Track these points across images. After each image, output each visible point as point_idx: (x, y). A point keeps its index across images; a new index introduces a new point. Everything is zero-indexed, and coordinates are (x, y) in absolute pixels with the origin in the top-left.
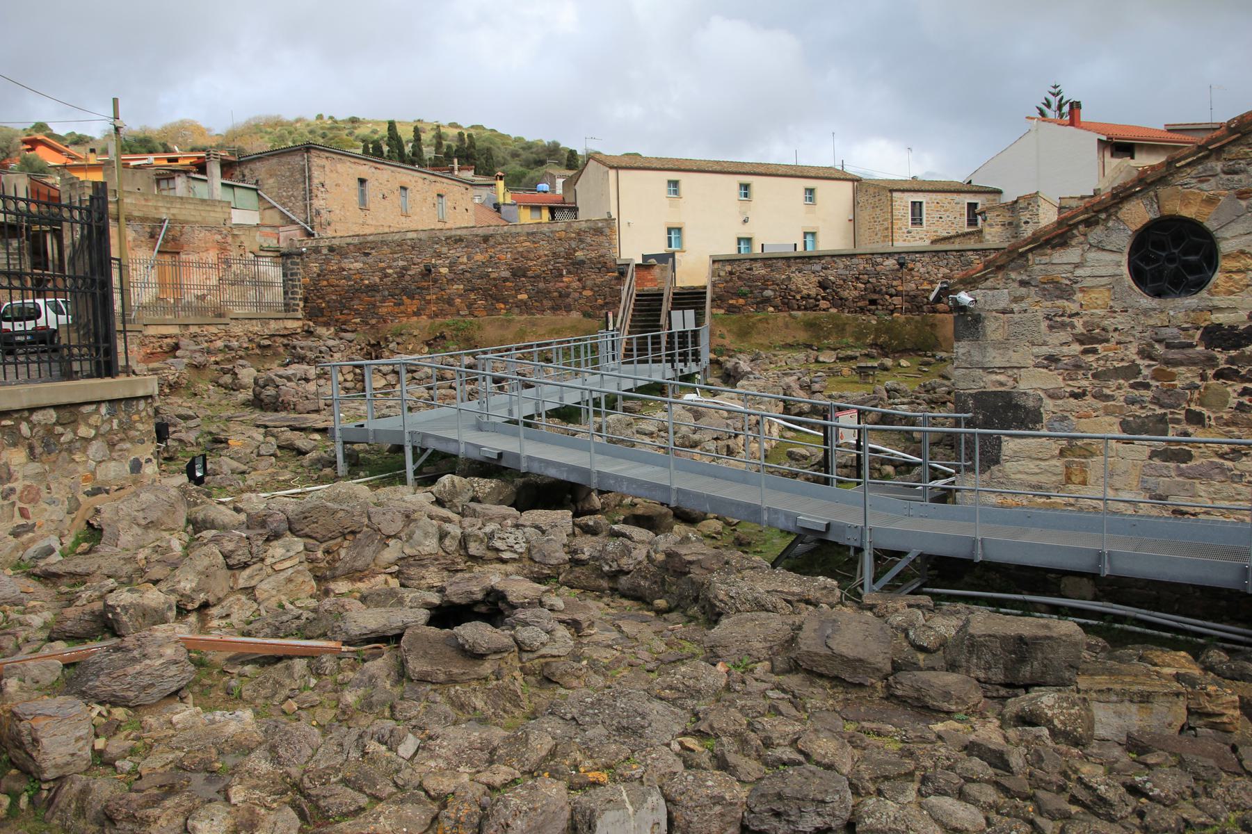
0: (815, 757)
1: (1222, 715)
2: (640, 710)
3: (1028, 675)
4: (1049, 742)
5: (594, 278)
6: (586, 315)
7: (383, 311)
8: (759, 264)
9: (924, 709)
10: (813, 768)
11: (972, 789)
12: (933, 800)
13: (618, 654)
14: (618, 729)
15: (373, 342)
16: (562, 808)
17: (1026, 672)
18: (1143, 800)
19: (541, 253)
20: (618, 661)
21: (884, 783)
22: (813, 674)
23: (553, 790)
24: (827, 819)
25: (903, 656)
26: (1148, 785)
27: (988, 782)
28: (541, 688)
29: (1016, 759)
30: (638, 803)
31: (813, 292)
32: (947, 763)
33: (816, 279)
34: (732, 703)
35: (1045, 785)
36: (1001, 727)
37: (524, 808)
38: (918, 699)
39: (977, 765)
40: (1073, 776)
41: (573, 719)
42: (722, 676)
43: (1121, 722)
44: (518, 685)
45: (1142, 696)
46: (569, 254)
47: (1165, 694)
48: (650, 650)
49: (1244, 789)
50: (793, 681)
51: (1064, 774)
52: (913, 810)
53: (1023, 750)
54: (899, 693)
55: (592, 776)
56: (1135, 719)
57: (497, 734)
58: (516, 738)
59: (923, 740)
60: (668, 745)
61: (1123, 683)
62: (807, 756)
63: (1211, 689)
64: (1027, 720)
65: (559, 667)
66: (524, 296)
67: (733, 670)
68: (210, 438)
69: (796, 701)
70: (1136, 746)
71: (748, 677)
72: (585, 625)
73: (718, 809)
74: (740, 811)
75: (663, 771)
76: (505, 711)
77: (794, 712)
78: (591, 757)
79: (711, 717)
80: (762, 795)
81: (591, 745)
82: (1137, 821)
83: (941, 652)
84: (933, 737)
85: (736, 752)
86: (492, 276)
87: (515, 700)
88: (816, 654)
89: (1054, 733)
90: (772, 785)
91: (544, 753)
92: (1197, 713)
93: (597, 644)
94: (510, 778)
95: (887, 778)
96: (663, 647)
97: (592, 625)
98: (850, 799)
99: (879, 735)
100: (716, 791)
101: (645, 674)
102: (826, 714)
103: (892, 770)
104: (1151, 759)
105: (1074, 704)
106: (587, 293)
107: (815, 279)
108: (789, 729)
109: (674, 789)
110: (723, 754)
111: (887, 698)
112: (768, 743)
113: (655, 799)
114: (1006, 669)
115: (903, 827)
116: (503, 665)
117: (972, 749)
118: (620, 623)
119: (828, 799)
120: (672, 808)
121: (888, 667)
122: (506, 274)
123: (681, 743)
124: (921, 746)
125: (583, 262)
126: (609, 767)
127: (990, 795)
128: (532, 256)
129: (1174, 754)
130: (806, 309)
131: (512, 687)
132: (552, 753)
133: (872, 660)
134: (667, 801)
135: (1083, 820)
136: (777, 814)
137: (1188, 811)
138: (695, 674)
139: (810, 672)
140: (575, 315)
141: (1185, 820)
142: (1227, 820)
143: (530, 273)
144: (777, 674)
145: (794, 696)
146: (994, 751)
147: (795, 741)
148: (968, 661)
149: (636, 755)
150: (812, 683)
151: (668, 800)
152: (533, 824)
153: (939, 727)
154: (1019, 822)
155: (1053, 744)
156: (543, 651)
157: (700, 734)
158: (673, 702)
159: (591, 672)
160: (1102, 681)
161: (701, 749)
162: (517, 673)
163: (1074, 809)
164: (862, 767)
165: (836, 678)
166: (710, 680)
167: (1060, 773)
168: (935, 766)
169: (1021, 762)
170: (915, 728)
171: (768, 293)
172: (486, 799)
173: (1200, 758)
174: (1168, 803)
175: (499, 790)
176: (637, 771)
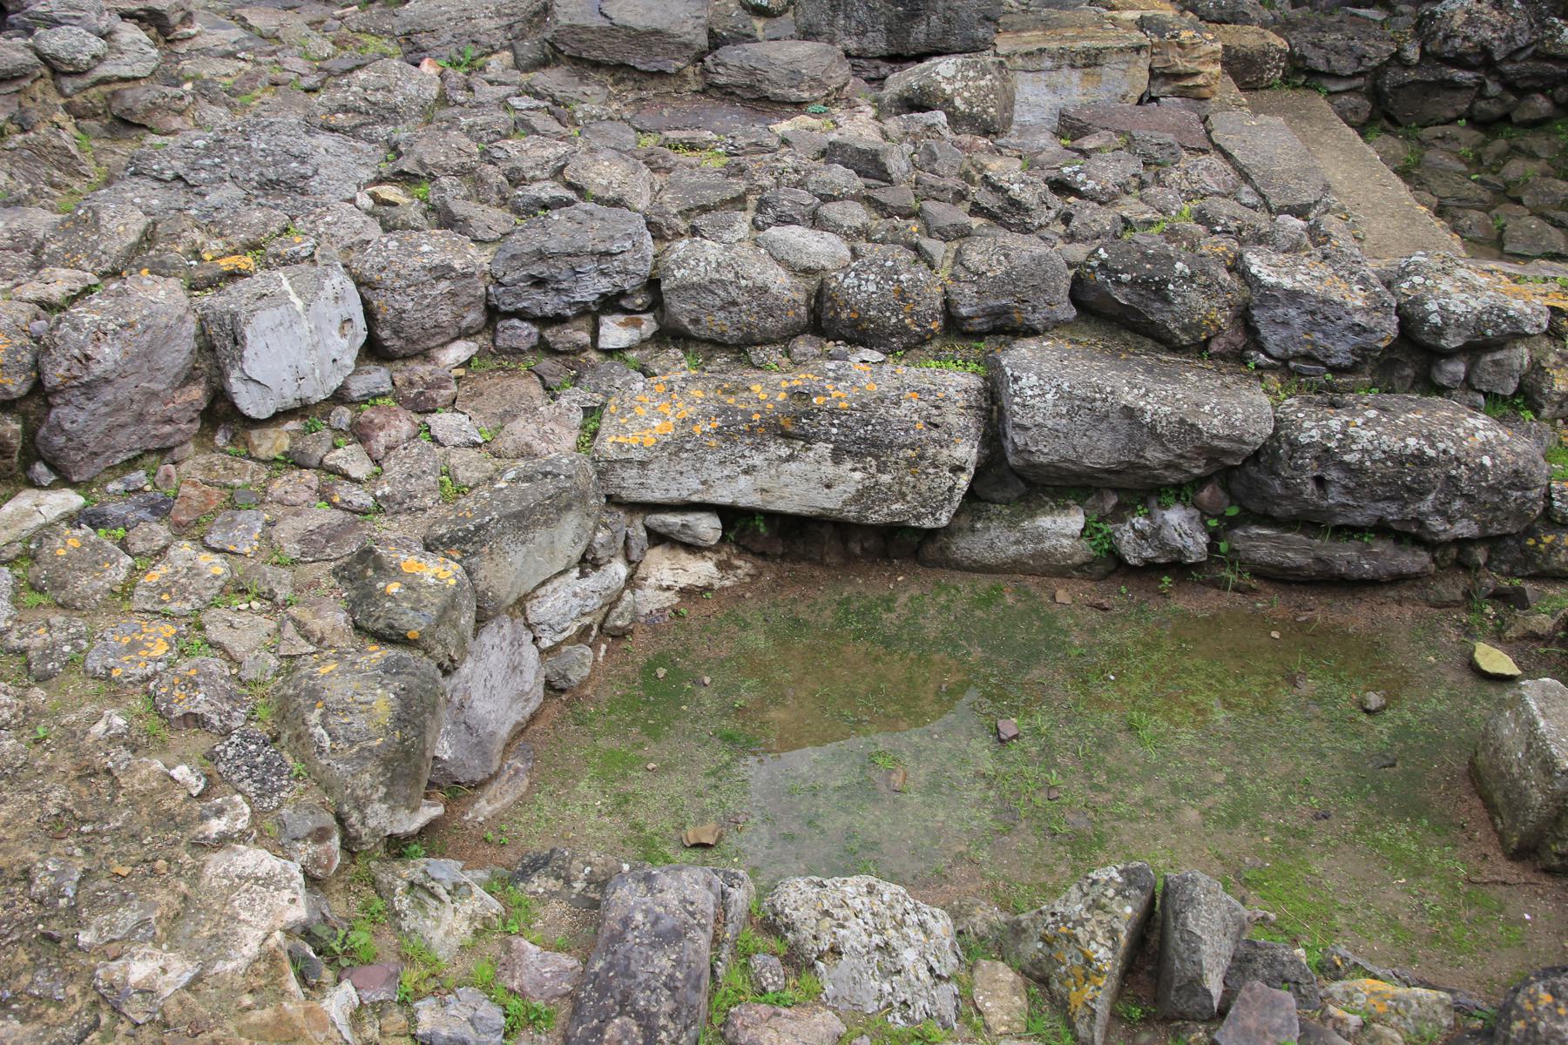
0: (593, 190)
1: (1197, 74)
2: (295, 150)
3: (922, 37)
4: (947, 133)
9: (761, 100)
10: (590, 206)
11: (832, 211)
12: (774, 232)
13: (248, 67)
14: (261, 186)
16: (181, 319)
17: (919, 33)
18: (1072, 199)
20: (252, 78)
21: (700, 215)
22: (585, 65)
23: (159, 295)
24: (617, 279)
25: (730, 24)
26: (1080, 177)
27: (854, 198)
28: (115, 140)
29: (897, 163)
30: (310, 295)
32: (794, 177)
34: (453, 123)
35: (936, 194)
36: (876, 118)
37: (111, 326)
38: (751, 87)
39: (840, 176)
40: (978, 177)
41: (178, 178)
42: (430, 82)
43: (1056, 100)
44: (68, 137)
45: (1088, 57)
47: (1121, 50)
48: (305, 55)
49: (1207, 169)
50: (551, 79)
51: (967, 177)
52: (746, 250)
53: (907, 147)
54: (721, 80)
55: (226, 264)
56: (1075, 91)
57: (40, 220)
58: (77, 222)
59: (760, 148)
60: (352, 200)
61: (1063, 38)
62: (580, 190)
63: (1185, 35)
64: (914, 103)
65: (137, 98)
67: (450, 71)
69: (558, 107)
70: (1070, 128)
71: (476, 80)
72: (175, 18)
73: (444, 286)
74: (481, 284)
75: (347, 241)
76: (53, 185)
77: (556, 127)
78: (221, 235)
79: (419, 149)
80: (513, 257)
81: (218, 216)
82: (1061, 229)
83: (790, 15)
84: (775, 143)
85: (466, 198)
87: (68, 163)
88: (585, 29)
89: (955, 120)
90: (528, 238)
91: (133, 239)
92: (1163, 74)
93: (205, 52)
94: (79, 286)
95: (705, 209)
96: (329, 49)
97: (188, 18)
98: (649, 246)
99: (692, 149)
100: (437, 259)
101: (303, 95)
102: (607, 125)
103: (713, 196)
104: (1088, 143)
105: (984, 72)
108: (549, 152)
109: (368, 263)
110: (445, 203)
111: (704, 92)
112: (516, 178)
113: (338, 280)
114: (889, 31)
115: (731, 276)
116: (29, 104)
117: (830, 153)
118: (245, 13)
119: (614, 249)
120: (369, 294)
121: (702, 40)
123: (373, 196)
124: (756, 157)
126: (253, 247)
127: (856, 215)
129: (1120, 133)
131: (56, 142)
132: (148, 237)
133: (675, 30)
134: (359, 285)
135: (987, 235)
136: (539, 282)
137: (1131, 207)
138: (384, 81)
139: (577, 60)
141: (1125, 220)
142: (1179, 212)
144: (525, 71)
145: (555, 103)
146: (864, 152)
147: (559, 171)
148: (831, 24)
149: (299, 222)
150: (583, 79)
151: (361, 283)
152: (133, 349)
153: (783, 127)
154: (897, 249)
155: (954, 136)
156: (102, 71)
157: (405, 178)
158: (353, 132)
159: (203, 102)
160: (1032, 39)
161: (407, 201)
162: (60, 117)
163: (976, 222)
164: (667, 197)
165: (622, 66)
166: (411, 89)
167: (960, 175)
168: (778, 185)
169: (904, 166)
170: (740, 128)
172: (38, 326)
173: (1155, 134)
174: (1104, 200)
175: (62, 309)
176: (303, 245)
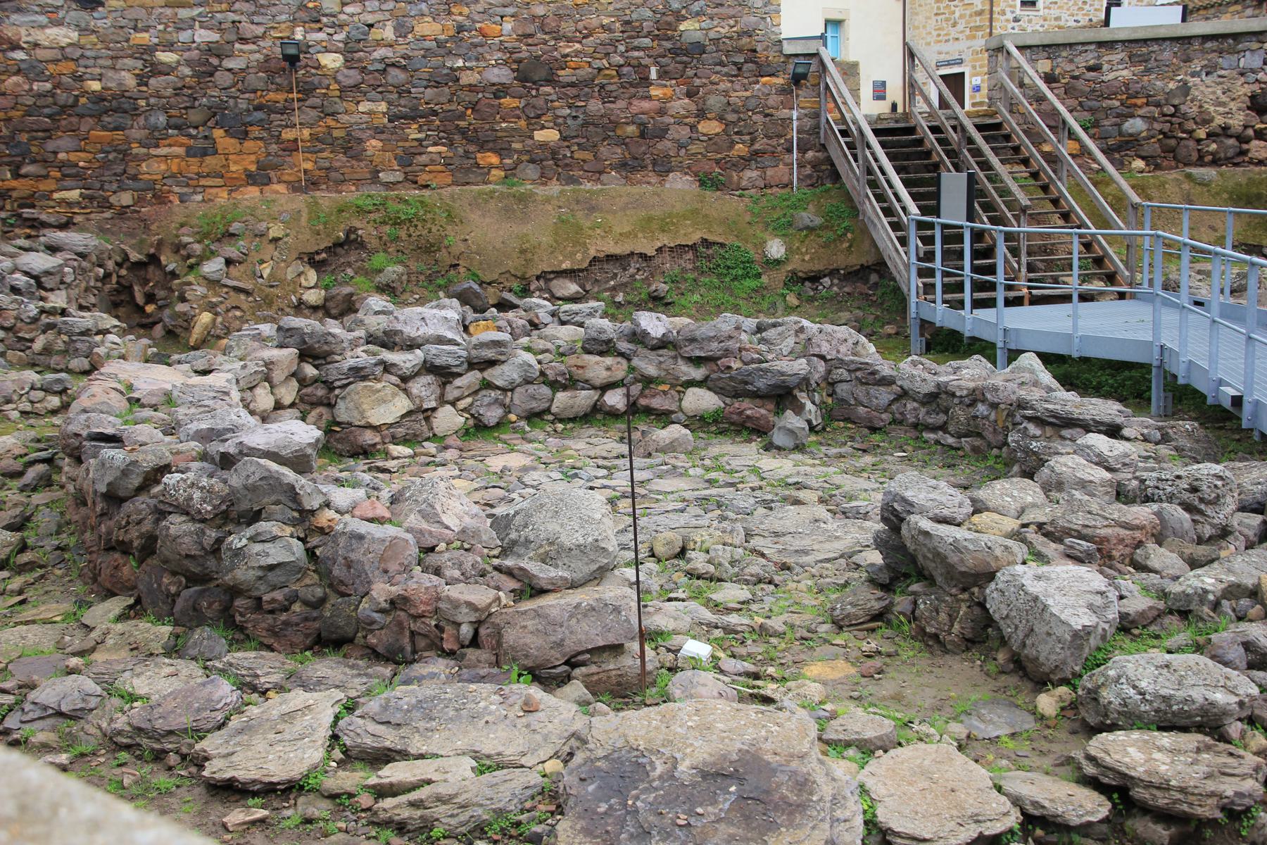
5: (726, 90)
6: (705, 181)
7: (152, 169)
8: (1117, 56)
15: (135, 256)
19: (594, 21)
26: (1068, 612)
31: (1237, 122)
33: (1248, 90)
46: (665, 28)
66: (548, 135)
68: (196, 334)
86: (466, 78)
106: (711, 127)
107: (1243, 90)
122: (500, 75)
125: (699, 48)
128: (567, 27)
130: (1215, 162)
140: (680, 183)
143: (565, 75)
171: (1135, 125)
